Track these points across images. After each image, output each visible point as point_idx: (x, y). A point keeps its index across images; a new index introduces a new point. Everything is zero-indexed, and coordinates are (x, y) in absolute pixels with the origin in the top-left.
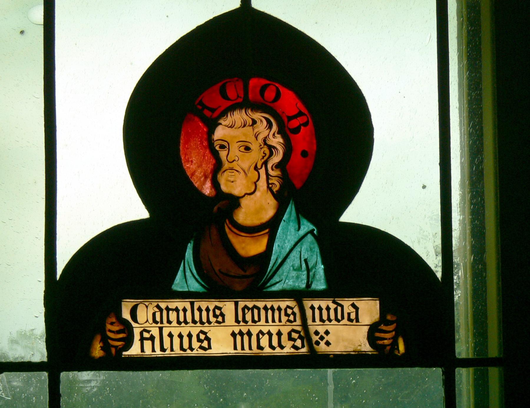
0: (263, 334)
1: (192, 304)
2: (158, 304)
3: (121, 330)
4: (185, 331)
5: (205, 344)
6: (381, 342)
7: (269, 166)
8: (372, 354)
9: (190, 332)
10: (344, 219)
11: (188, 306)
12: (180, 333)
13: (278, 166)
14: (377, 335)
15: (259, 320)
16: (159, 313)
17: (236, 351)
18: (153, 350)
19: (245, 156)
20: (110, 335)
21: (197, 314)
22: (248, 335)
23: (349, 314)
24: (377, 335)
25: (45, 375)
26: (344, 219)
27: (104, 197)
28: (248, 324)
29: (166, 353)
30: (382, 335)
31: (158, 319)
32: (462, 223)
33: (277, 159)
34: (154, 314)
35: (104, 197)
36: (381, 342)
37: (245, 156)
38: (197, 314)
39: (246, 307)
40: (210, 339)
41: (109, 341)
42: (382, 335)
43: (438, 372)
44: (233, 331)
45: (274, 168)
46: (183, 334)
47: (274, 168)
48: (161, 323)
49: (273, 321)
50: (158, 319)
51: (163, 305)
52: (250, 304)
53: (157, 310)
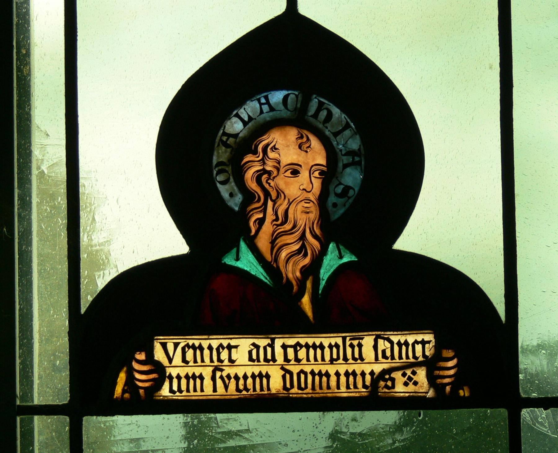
1: (344, 339)
3: (151, 369)
4: (342, 369)
5: (389, 383)
8: (409, 396)
10: (401, 244)
11: (340, 341)
14: (437, 372)
15: (338, 358)
16: (255, 349)
17: (188, 394)
18: (215, 390)
20: (138, 376)
21: (349, 351)
22: (319, 376)
23: (384, 352)
24: (437, 372)
26: (401, 244)
28: (190, 364)
29: (249, 393)
30: (442, 373)
31: (254, 357)
34: (250, 352)
37: (294, 166)
38: (349, 351)
39: (187, 345)
41: (137, 383)
43: (504, 412)
44: (347, 371)
46: (239, 375)
48: (258, 362)
49: (316, 360)
50: (254, 357)
51: (395, 339)
52: (291, 342)
53: (252, 347)
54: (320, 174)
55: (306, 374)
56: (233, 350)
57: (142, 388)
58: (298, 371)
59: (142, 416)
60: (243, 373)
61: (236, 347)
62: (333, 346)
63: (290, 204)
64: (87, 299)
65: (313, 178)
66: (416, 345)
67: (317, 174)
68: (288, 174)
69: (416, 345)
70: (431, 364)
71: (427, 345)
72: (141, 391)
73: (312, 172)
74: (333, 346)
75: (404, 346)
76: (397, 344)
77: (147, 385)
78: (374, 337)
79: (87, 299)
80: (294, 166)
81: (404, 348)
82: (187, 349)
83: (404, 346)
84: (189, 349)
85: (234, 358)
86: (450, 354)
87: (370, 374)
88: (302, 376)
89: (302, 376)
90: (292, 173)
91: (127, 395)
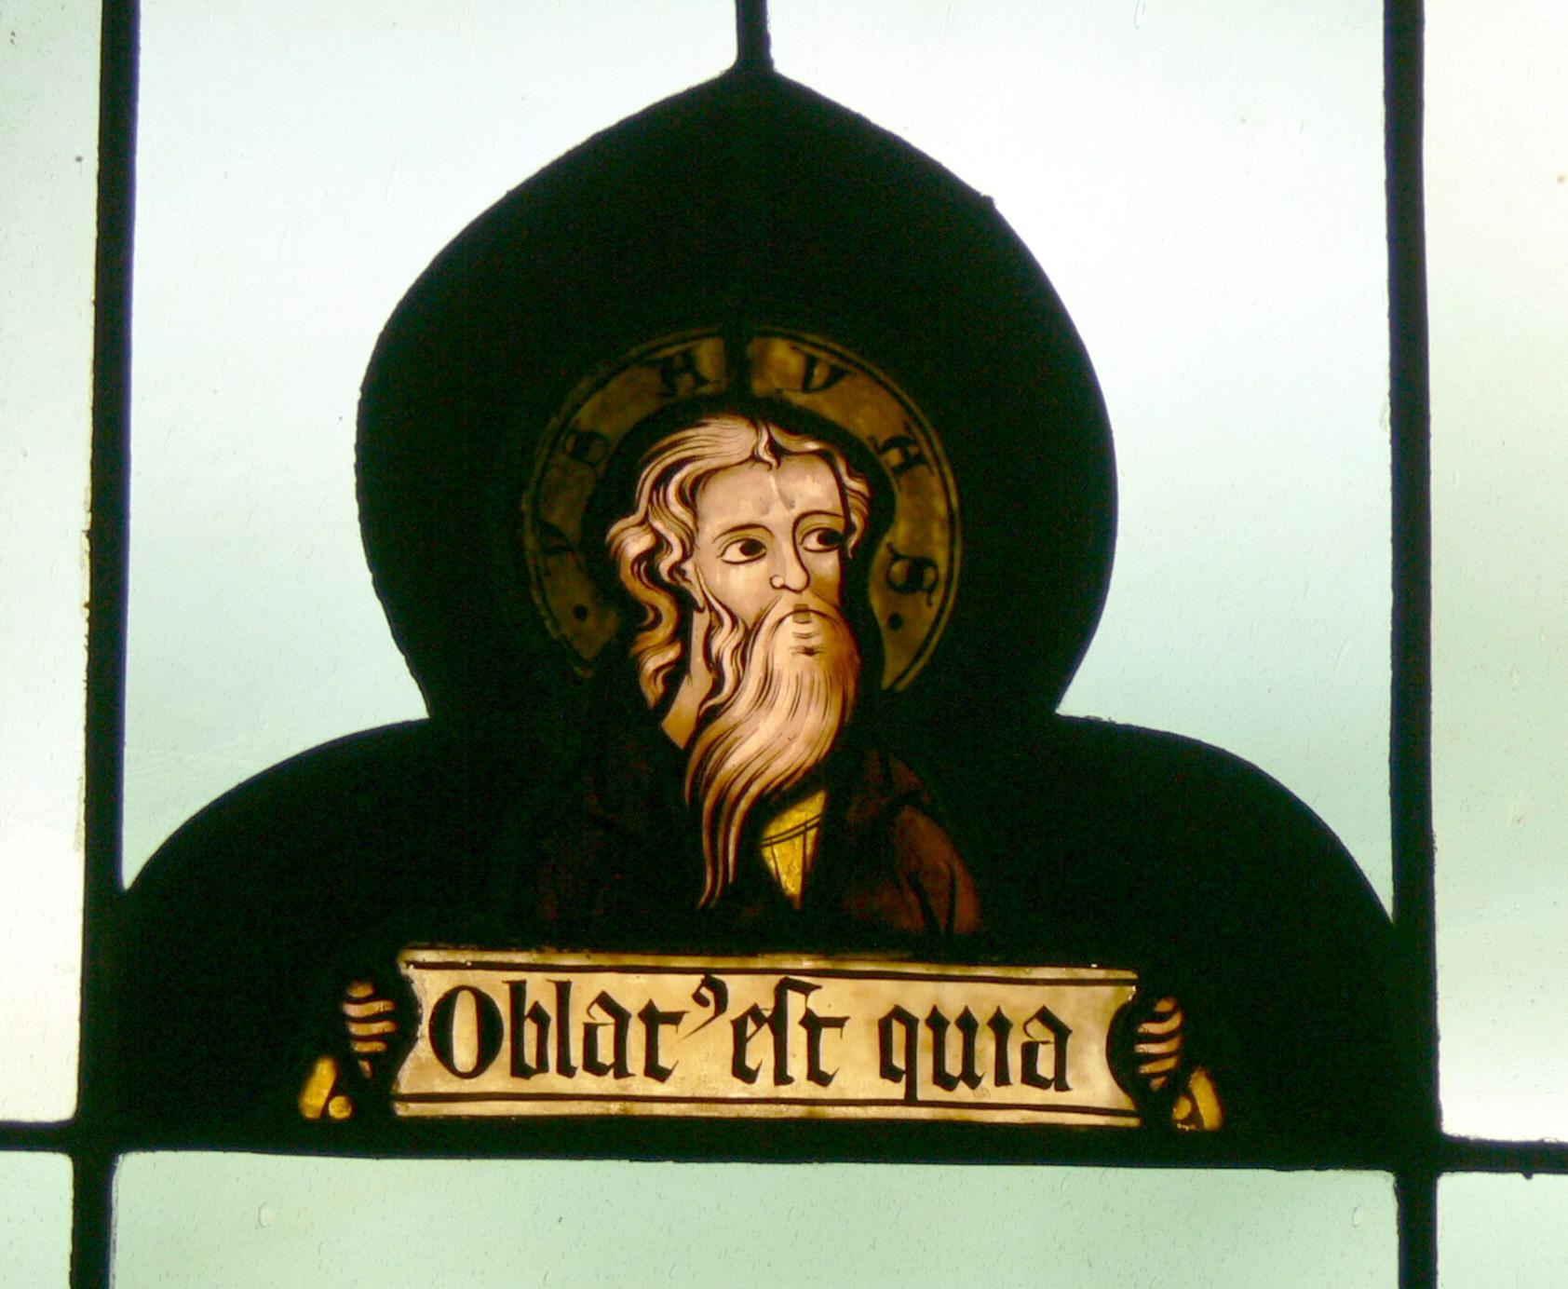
6: (379, 1006)
10: (1079, 700)
20: (355, 1029)
27: (294, 650)
35: (294, 650)
37: (750, 556)
54: (820, 540)
55: (910, 1022)
57: (366, 1056)
58: (883, 1011)
60: (994, 1010)
61: (838, 1023)
63: (750, 634)
64: (135, 857)
65: (806, 556)
67: (812, 542)
68: (734, 553)
72: (365, 1065)
73: (799, 539)
77: (377, 1046)
79: (135, 857)
80: (750, 556)
82: (751, 1027)
84: (759, 1027)
87: (642, 1016)
88: (898, 1031)
89: (898, 1031)
90: (743, 550)
91: (365, 1065)
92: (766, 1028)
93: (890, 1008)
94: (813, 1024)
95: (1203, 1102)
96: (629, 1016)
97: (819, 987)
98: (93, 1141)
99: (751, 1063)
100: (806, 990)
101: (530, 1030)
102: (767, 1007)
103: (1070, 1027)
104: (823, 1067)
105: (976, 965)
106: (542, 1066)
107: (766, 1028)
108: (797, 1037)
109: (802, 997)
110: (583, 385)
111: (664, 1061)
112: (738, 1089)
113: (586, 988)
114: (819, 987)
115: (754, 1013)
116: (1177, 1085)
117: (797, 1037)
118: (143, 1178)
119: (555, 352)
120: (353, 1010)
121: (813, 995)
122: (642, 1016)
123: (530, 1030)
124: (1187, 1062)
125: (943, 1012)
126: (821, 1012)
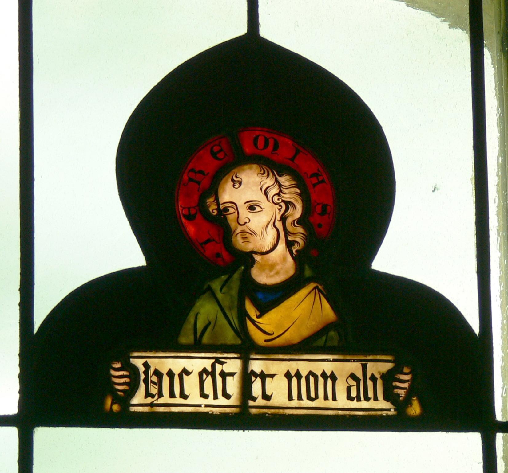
0: (188, 373)
2: (146, 362)
6: (125, 373)
7: (289, 221)
9: (298, 370)
12: (324, 371)
13: (300, 221)
19: (258, 206)
20: (113, 373)
25: (317, 181)
27: (93, 238)
30: (398, 384)
32: (211, 354)
33: (297, 213)
35: (93, 238)
36: (125, 373)
37: (258, 206)
40: (337, 379)
42: (398, 384)
45: (296, 225)
47: (296, 225)
56: (268, 380)
59: (19, 145)
61: (272, 376)
62: (328, 377)
64: (40, 316)
66: (184, 376)
69: (184, 376)
70: (388, 379)
71: (229, 379)
74: (328, 377)
75: (329, 380)
76: (370, 379)
78: (213, 361)
79: (40, 316)
81: (294, 381)
82: (205, 376)
83: (329, 380)
85: (268, 393)
86: (406, 370)
87: (167, 374)
92: (210, 377)
93: (202, 368)
94: (224, 375)
95: (415, 409)
96: (302, 377)
97: (226, 363)
98: (26, 422)
99: (206, 392)
100: (222, 363)
101: (370, 384)
102: (209, 369)
103: (339, 378)
104: (267, 393)
105: (302, 354)
106: (317, 397)
107: (210, 377)
108: (219, 380)
109: (221, 366)
110: (259, 129)
111: (186, 393)
112: (203, 401)
113: (154, 364)
114: (226, 363)
115: (205, 370)
116: (408, 401)
117: (219, 380)
118: (43, 435)
119: (243, 117)
120: (113, 373)
121: (225, 365)
122: (167, 374)
123: (370, 384)
124: (410, 392)
125: (174, 371)
126: (227, 370)
